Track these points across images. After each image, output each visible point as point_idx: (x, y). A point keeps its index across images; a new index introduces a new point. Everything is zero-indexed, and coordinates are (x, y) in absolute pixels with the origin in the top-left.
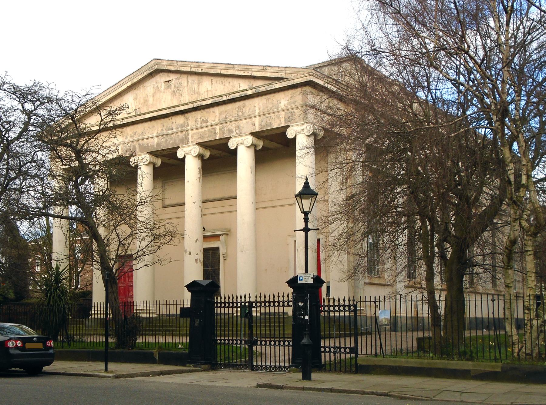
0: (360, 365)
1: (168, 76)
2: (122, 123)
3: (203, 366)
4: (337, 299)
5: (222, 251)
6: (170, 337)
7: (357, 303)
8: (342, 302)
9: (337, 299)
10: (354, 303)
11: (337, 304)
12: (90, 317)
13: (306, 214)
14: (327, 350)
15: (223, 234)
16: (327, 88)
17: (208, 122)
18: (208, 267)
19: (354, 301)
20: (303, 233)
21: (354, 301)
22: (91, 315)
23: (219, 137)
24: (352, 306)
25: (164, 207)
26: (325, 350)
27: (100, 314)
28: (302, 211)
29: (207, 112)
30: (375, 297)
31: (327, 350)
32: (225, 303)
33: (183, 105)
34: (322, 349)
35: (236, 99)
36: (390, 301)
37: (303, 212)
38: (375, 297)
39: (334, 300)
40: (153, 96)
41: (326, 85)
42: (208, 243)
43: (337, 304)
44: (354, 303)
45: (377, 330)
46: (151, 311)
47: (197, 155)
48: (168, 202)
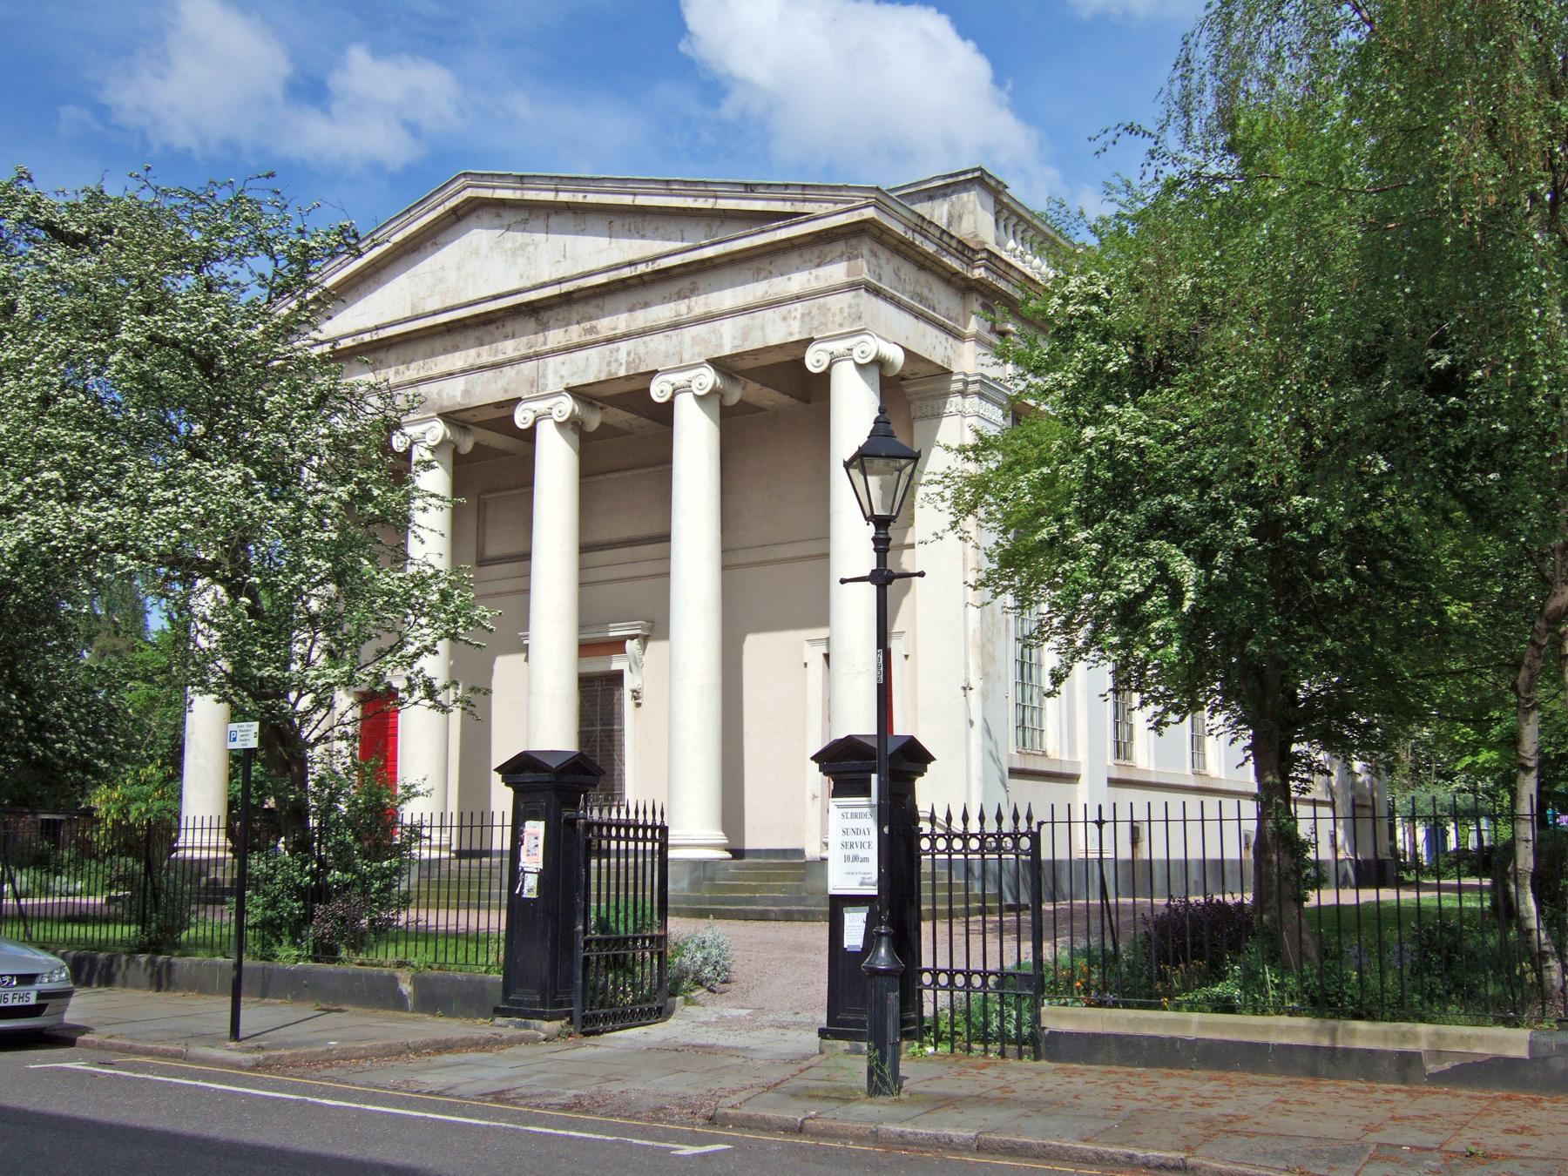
0: (1055, 1035)
1: (498, 215)
2: (375, 338)
3: (546, 1025)
4: (941, 816)
5: (630, 682)
6: (444, 928)
7: (1040, 824)
8: (957, 826)
9: (941, 816)
10: (1030, 828)
11: (994, 830)
12: (174, 855)
13: (881, 523)
14: (943, 979)
15: (632, 637)
16: (913, 243)
17: (597, 333)
18: (593, 725)
19: (1029, 818)
20: (870, 590)
21: (1029, 818)
22: (176, 849)
23: (627, 370)
24: (1024, 835)
25: (482, 561)
26: (935, 981)
27: (209, 848)
28: (868, 513)
29: (597, 306)
30: (1100, 807)
31: (943, 979)
32: (645, 827)
33: (535, 288)
34: (927, 978)
35: (675, 272)
36: (1335, 818)
37: (872, 518)
38: (1100, 807)
39: (932, 819)
40: (458, 269)
41: (909, 236)
42: (593, 659)
43: (994, 830)
44: (1030, 828)
45: (1107, 923)
46: (213, 844)
47: (568, 420)
48: (492, 550)
